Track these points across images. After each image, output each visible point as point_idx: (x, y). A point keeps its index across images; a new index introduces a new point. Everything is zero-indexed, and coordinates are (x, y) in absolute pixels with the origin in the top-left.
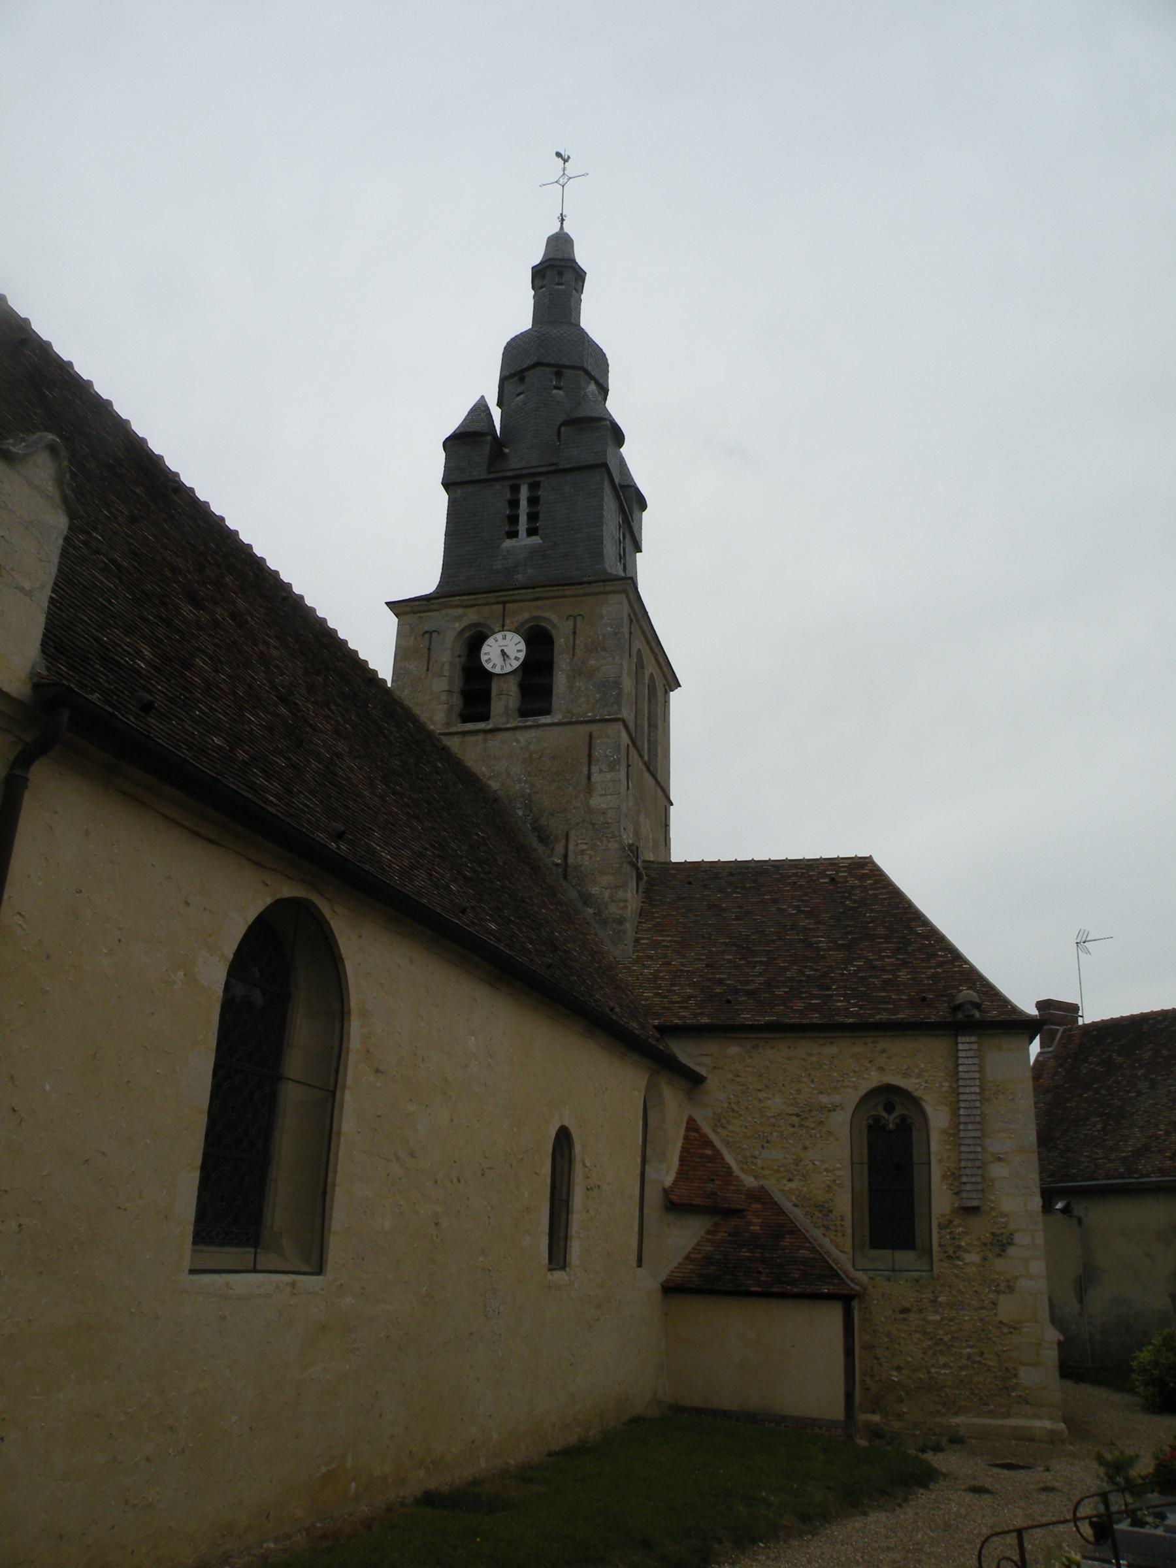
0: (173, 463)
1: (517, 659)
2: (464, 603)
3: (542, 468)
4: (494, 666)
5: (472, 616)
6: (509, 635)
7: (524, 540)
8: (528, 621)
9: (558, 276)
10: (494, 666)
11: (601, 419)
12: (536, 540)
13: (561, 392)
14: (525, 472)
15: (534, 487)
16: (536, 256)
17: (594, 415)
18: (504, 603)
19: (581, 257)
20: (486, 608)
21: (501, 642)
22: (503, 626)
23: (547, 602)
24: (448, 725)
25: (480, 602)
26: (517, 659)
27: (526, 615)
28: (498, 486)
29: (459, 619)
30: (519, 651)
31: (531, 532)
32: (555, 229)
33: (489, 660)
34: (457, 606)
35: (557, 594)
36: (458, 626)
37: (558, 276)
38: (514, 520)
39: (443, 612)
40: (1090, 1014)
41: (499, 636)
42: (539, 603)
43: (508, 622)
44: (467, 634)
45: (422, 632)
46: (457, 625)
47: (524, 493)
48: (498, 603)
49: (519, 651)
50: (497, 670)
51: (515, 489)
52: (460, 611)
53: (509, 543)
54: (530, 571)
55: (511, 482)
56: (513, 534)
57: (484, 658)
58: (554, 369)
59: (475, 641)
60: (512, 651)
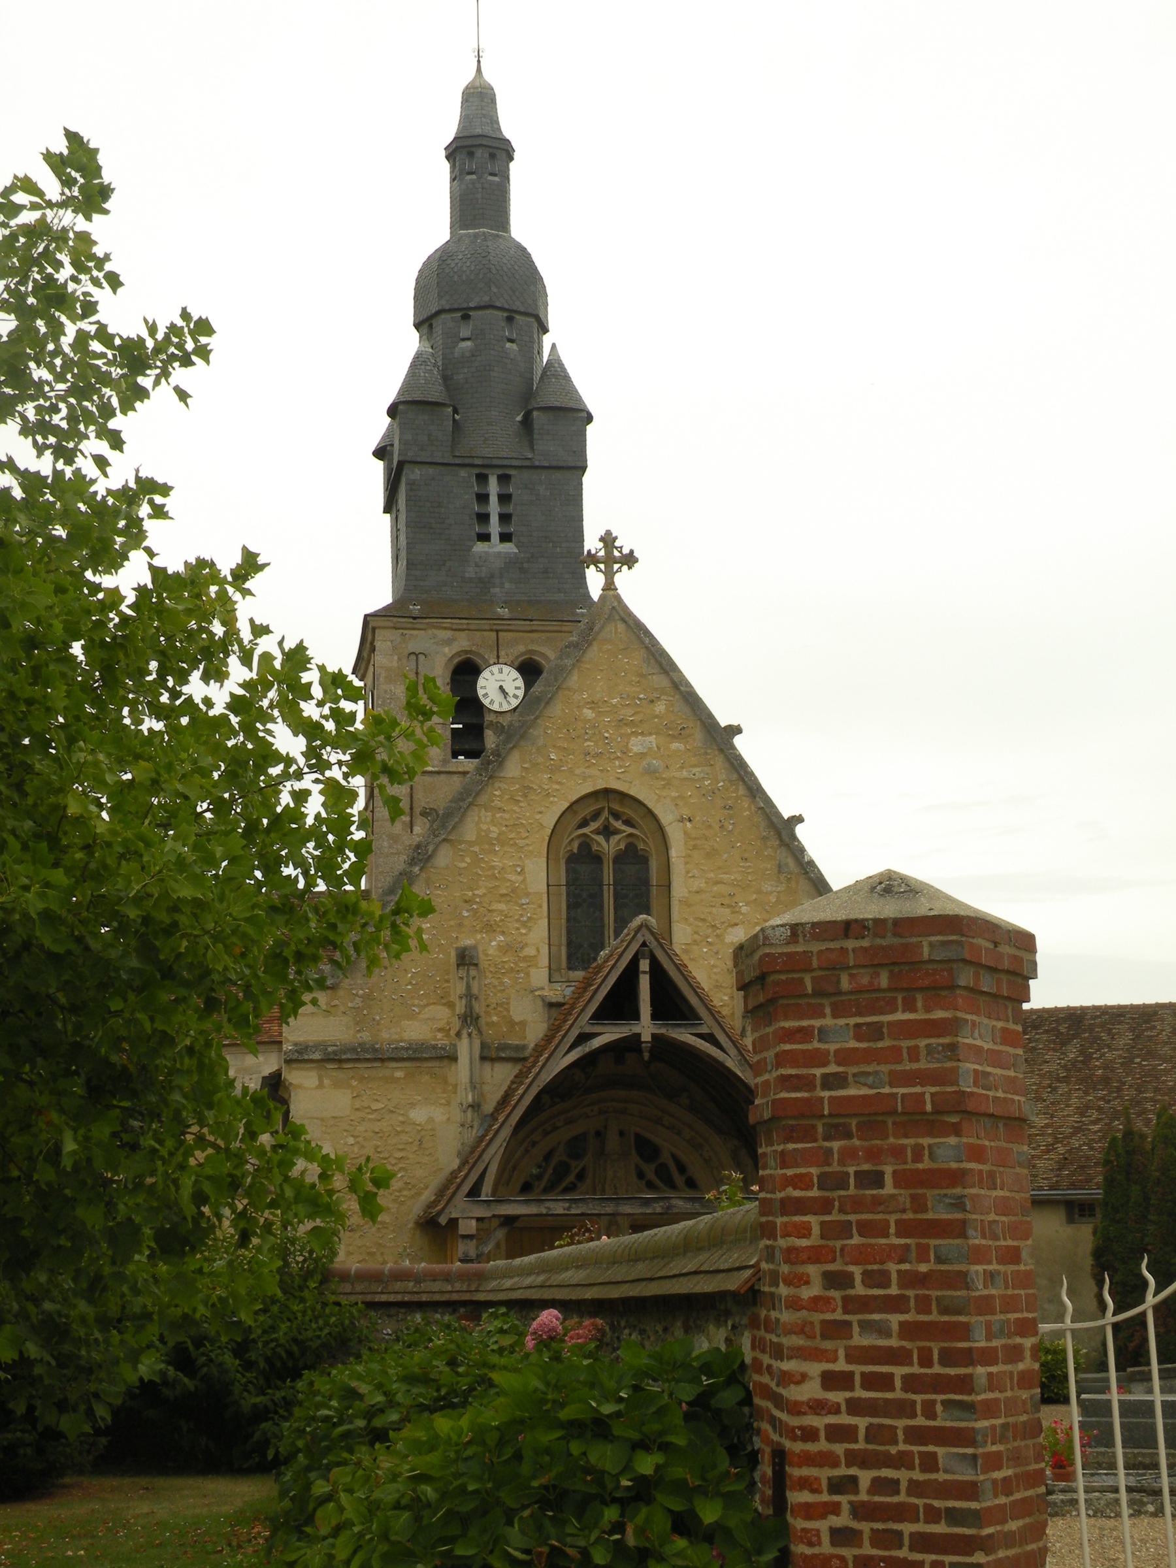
0: (1148, 1002)
1: (515, 696)
2: (454, 627)
3: (482, 430)
4: (492, 702)
5: (462, 643)
6: (506, 669)
7: (496, 547)
8: (522, 654)
9: (479, 158)
10: (492, 702)
11: (582, 410)
12: (509, 548)
13: (514, 346)
14: (495, 462)
15: (504, 479)
16: (448, 128)
17: (571, 405)
18: (497, 631)
19: (510, 126)
20: (478, 633)
21: (498, 676)
22: (498, 657)
23: (544, 636)
24: (445, 762)
25: (472, 627)
26: (515, 696)
27: (522, 648)
28: (463, 473)
29: (449, 642)
30: (517, 688)
31: (505, 538)
32: (469, 76)
33: (486, 695)
34: (445, 628)
35: (555, 628)
36: (448, 651)
37: (479, 158)
38: (484, 518)
39: (430, 632)
40: (1031, 982)
41: (495, 668)
42: (535, 635)
43: (502, 653)
44: (456, 661)
45: (407, 652)
46: (446, 650)
47: (493, 487)
48: (491, 630)
49: (517, 688)
50: (495, 707)
51: (482, 479)
52: (449, 634)
53: (480, 547)
54: (507, 585)
55: (477, 471)
56: (485, 537)
57: (480, 692)
58: (505, 315)
59: (466, 672)
60: (510, 689)
